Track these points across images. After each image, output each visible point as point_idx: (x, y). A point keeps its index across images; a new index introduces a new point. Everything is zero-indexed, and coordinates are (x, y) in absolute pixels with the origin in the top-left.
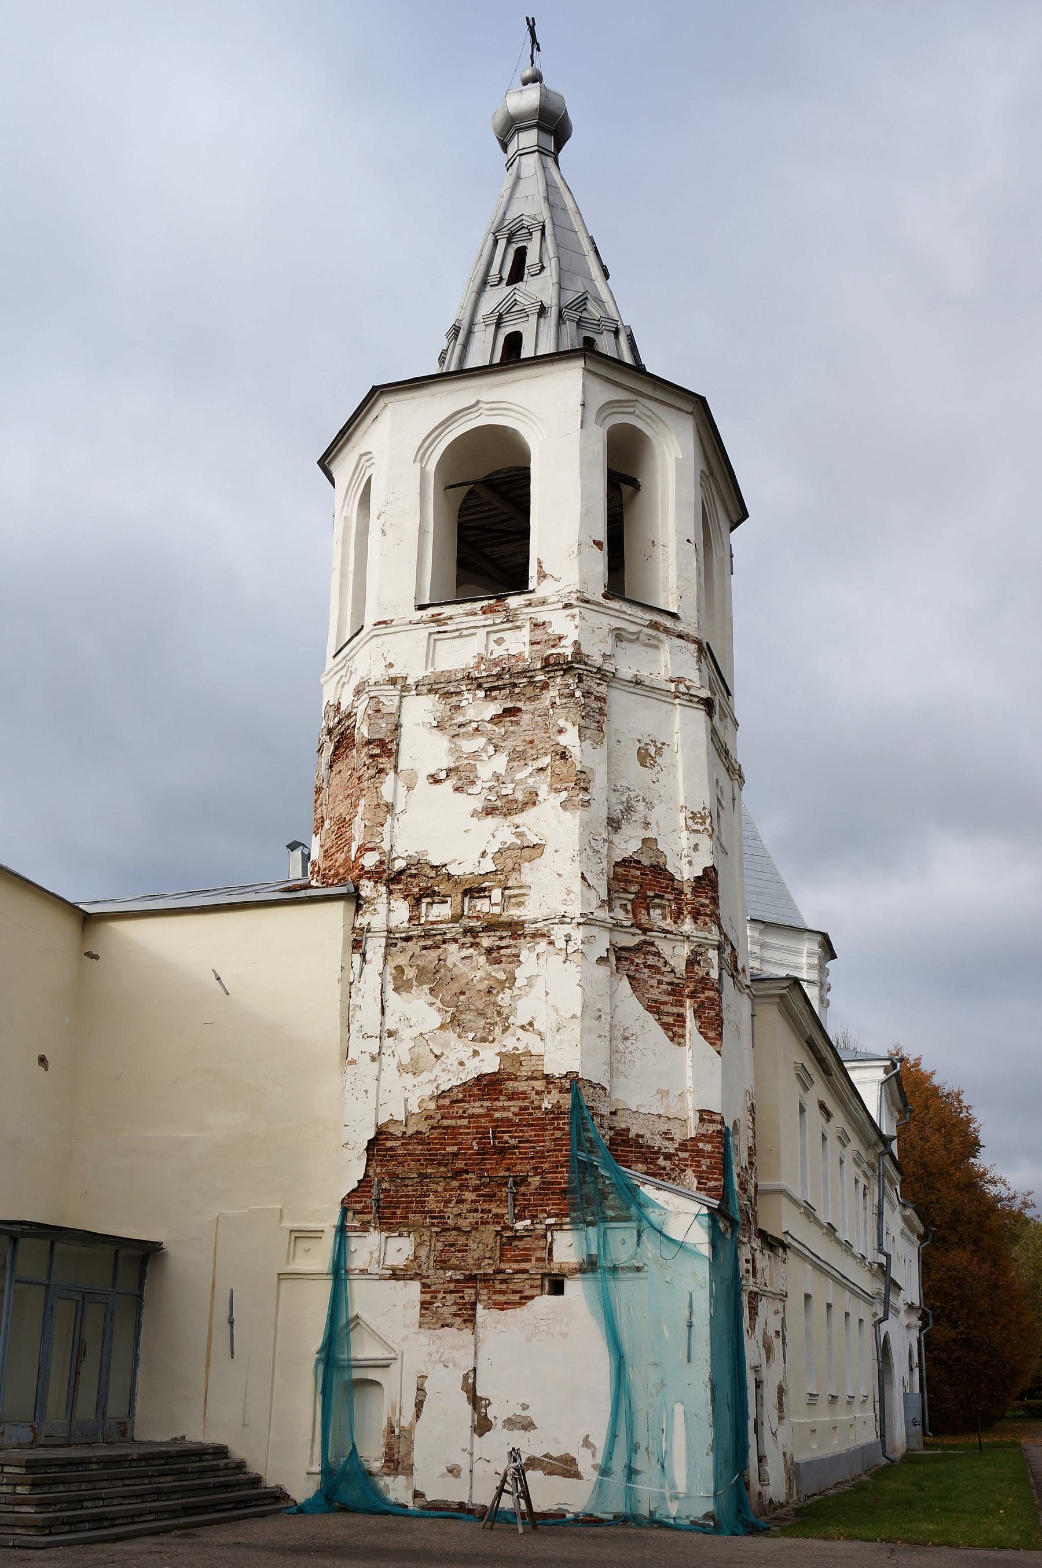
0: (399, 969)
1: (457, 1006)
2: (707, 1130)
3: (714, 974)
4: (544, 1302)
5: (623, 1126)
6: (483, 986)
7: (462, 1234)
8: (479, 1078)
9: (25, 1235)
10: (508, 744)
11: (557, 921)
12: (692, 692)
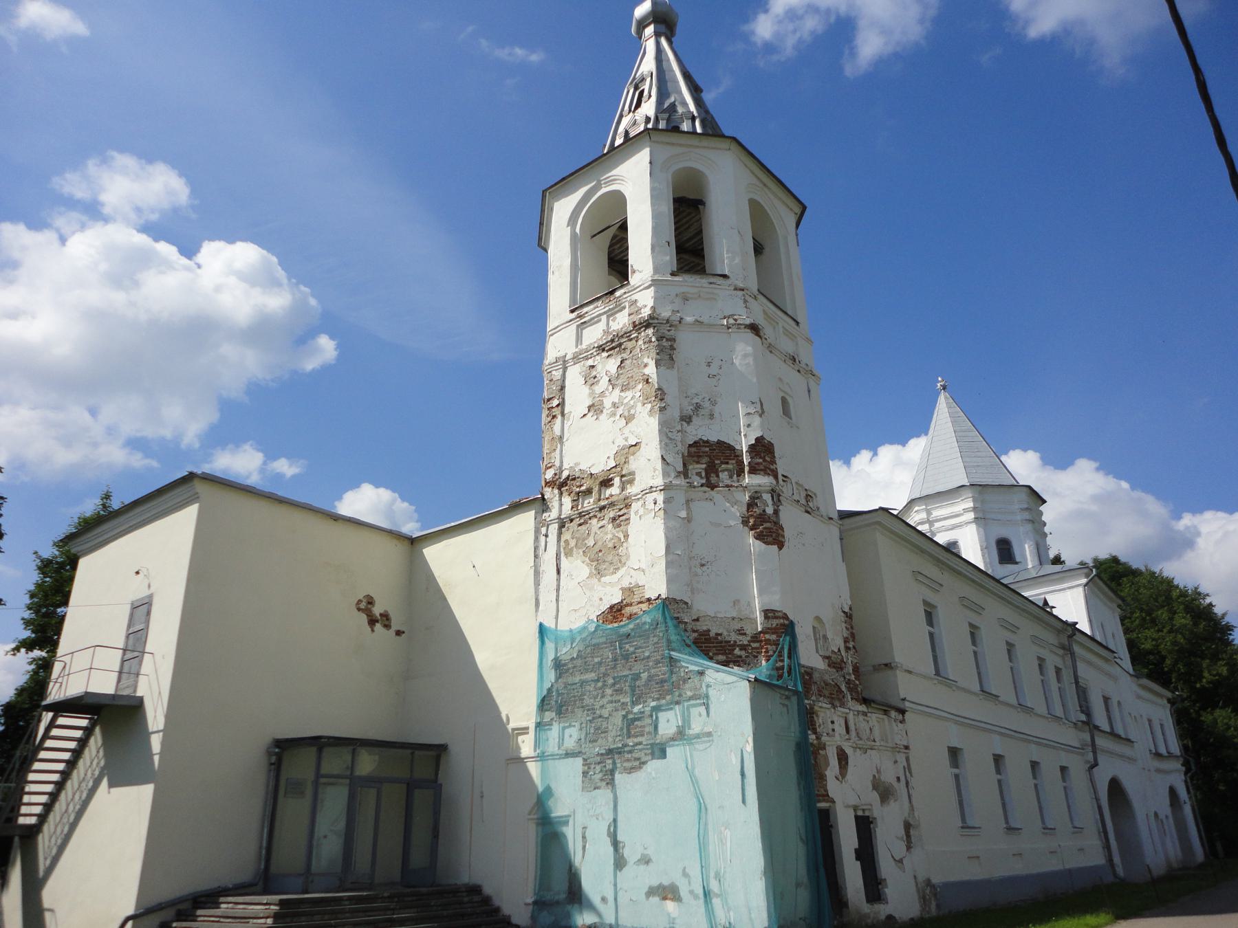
0: (566, 541)
1: (598, 561)
2: (772, 624)
3: (770, 510)
4: (654, 766)
5: (705, 628)
6: (611, 545)
7: (604, 720)
8: (612, 607)
9: (330, 745)
10: (620, 381)
11: (647, 491)
12: (738, 322)
